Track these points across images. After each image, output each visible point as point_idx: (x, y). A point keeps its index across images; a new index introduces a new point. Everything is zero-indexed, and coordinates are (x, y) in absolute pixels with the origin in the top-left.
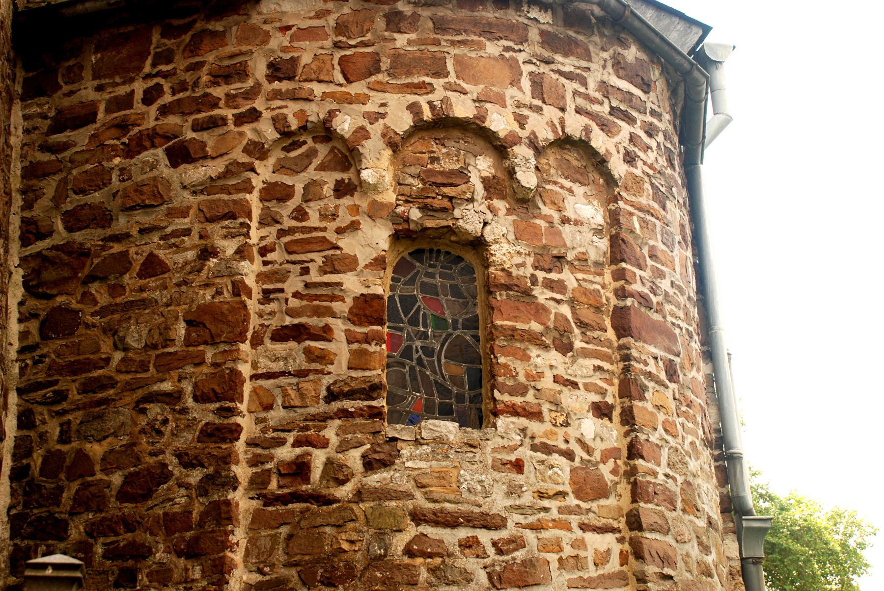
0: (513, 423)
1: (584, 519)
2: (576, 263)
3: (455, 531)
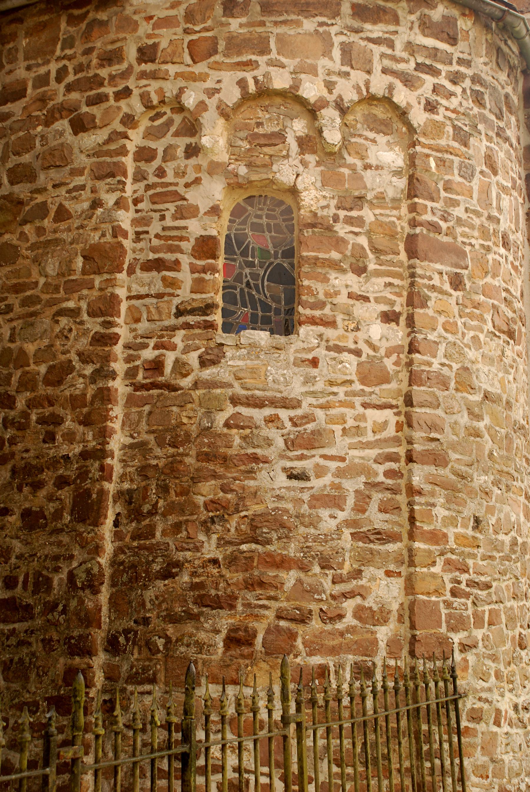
0: (312, 330)
1: (367, 399)
2: (375, 201)
3: (262, 410)
